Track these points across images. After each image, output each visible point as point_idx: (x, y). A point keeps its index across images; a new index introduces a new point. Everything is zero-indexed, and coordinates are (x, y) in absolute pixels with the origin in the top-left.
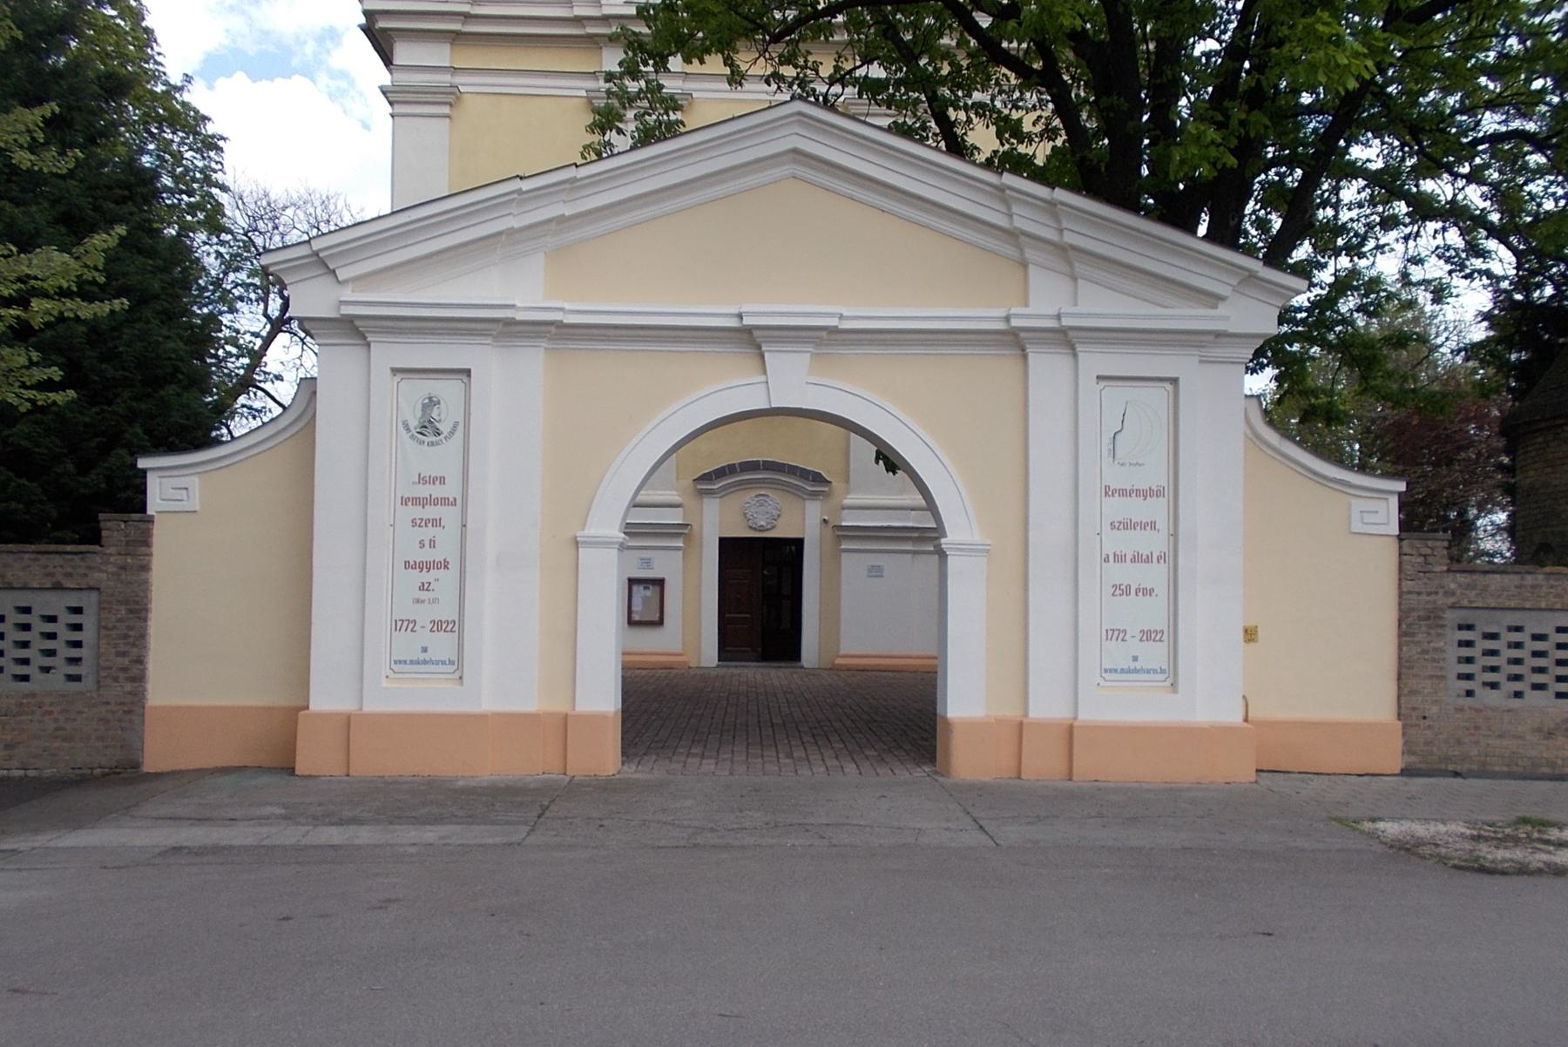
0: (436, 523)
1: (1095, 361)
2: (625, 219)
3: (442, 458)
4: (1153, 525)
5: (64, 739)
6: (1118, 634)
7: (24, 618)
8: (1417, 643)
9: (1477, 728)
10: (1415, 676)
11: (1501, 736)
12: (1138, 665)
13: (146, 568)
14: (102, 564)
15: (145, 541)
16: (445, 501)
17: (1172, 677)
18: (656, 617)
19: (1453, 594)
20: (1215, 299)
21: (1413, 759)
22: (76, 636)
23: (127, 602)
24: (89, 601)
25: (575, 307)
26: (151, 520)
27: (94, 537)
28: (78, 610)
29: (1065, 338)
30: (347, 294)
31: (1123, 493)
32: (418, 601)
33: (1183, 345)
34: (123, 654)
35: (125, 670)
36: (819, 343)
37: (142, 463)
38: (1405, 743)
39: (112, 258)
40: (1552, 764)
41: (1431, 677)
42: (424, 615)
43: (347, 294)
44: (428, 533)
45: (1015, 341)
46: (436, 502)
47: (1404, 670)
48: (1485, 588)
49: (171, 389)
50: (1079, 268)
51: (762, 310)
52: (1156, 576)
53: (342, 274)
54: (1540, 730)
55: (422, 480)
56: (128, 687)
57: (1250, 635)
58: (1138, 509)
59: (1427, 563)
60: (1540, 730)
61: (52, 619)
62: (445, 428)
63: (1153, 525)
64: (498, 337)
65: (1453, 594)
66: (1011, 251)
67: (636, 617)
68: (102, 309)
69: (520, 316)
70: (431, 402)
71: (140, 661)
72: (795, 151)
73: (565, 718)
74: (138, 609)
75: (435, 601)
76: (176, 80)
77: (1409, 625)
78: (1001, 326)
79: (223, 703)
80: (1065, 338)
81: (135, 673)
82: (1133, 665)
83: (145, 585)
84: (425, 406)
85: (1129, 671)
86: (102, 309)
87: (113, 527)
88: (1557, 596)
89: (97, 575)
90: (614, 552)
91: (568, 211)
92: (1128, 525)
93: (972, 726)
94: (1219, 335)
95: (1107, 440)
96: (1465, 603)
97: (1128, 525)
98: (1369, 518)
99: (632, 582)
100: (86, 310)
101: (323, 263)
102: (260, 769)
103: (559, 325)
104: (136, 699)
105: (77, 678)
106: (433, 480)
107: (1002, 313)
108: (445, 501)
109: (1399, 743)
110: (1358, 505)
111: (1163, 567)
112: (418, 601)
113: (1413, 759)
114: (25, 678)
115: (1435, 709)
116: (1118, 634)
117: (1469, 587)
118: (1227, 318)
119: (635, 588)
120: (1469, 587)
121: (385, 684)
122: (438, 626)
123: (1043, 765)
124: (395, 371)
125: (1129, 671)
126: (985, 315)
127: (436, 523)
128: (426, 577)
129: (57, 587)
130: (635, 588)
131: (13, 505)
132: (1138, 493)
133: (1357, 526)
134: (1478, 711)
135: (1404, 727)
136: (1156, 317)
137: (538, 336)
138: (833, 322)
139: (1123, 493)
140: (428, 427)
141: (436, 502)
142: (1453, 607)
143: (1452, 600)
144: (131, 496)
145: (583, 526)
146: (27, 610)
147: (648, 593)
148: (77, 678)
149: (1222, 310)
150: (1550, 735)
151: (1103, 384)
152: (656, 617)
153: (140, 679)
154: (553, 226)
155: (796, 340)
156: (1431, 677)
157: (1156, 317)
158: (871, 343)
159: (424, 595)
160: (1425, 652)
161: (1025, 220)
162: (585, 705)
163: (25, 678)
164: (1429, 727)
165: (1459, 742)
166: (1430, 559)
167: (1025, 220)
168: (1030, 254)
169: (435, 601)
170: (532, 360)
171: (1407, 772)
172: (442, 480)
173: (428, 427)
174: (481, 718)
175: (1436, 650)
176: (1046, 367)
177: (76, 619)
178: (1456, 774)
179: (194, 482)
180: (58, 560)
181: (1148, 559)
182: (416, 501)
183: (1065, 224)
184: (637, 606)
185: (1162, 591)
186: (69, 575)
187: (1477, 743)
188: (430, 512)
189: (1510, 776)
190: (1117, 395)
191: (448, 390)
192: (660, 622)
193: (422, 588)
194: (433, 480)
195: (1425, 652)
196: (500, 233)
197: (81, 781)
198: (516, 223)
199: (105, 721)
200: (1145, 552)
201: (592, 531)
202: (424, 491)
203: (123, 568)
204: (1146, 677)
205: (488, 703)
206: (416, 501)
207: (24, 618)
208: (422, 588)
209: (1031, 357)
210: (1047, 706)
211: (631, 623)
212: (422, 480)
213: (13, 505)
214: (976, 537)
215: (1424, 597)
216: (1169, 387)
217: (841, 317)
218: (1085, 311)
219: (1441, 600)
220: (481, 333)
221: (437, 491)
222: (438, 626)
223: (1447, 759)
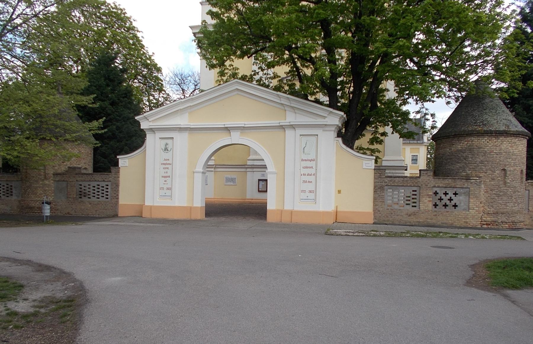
0: (168, 168)
1: (300, 131)
2: (212, 102)
3: (168, 155)
4: (312, 167)
5: (106, 210)
6: (304, 191)
7: (98, 187)
8: (378, 194)
9: (392, 214)
10: (377, 201)
11: (398, 216)
12: (308, 198)
13: (119, 177)
14: (111, 176)
15: (118, 172)
16: (169, 164)
17: (315, 200)
18: (266, 190)
19: (387, 183)
20: (325, 117)
21: (376, 220)
22: (107, 190)
23: (115, 184)
24: (109, 183)
25: (193, 125)
26: (119, 168)
27: (110, 172)
28: (107, 185)
29: (293, 127)
30: (151, 124)
31: (305, 160)
32: (164, 184)
33: (320, 127)
34: (115, 194)
35: (115, 197)
36: (242, 130)
37: (118, 157)
38: (374, 217)
39: (104, 122)
40: (410, 222)
41: (380, 202)
42: (165, 187)
43: (151, 124)
44: (166, 170)
45: (282, 127)
46: (167, 164)
47: (375, 199)
48: (394, 181)
49: (134, 138)
50: (296, 111)
51: (229, 123)
52: (312, 178)
53: (150, 120)
54: (407, 214)
55: (165, 160)
56: (116, 200)
57: (339, 192)
58: (309, 164)
59: (380, 175)
60: (407, 214)
61: (103, 187)
62: (169, 149)
63: (312, 167)
64: (179, 130)
65: (387, 183)
66: (283, 108)
67: (260, 190)
68: (103, 131)
69: (182, 127)
70: (167, 144)
71: (118, 195)
72: (237, 89)
73: (191, 207)
74: (117, 185)
75: (167, 184)
76: (150, 54)
77: (376, 190)
78: (278, 125)
79: (128, 203)
80: (293, 127)
81: (116, 197)
82: (307, 198)
83: (119, 180)
84: (165, 145)
85: (306, 199)
86: (103, 131)
87: (113, 169)
88: (412, 183)
89: (110, 179)
90: (201, 174)
91: (192, 105)
92: (307, 167)
93: (272, 211)
94: (326, 125)
95: (302, 149)
96: (389, 185)
97: (307, 167)
98: (367, 165)
99: (259, 180)
100: (100, 132)
101: (146, 118)
102: (138, 216)
103: (190, 128)
104: (117, 202)
105: (107, 198)
106: (167, 160)
107: (278, 122)
108: (169, 164)
109: (373, 216)
110: (364, 162)
111: (314, 176)
112: (164, 184)
113: (376, 220)
114: (99, 198)
115: (381, 209)
116: (304, 191)
117: (390, 181)
118: (327, 122)
119: (260, 182)
120: (390, 181)
121: (158, 200)
122: (168, 189)
123: (286, 219)
124: (160, 138)
125: (306, 199)
126: (275, 122)
127: (168, 168)
128: (166, 179)
129: (104, 181)
130: (260, 182)
131: (101, 164)
132: (309, 160)
133: (364, 167)
134: (392, 210)
135: (374, 213)
136: (315, 122)
137: (187, 130)
138: (243, 125)
139: (305, 160)
140: (166, 149)
141: (167, 164)
142: (386, 185)
143: (386, 184)
144: (116, 164)
145: (195, 169)
146: (99, 185)
147: (263, 183)
148: (107, 198)
149: (326, 119)
150: (410, 215)
151: (302, 136)
152: (266, 190)
153: (118, 199)
154: (189, 108)
155: (237, 129)
156: (380, 202)
157: (315, 122)
158: (253, 129)
159: (165, 183)
160: (380, 196)
161: (283, 101)
162: (195, 205)
163: (99, 198)
164: (380, 213)
165: (387, 217)
166: (381, 174)
167: (283, 101)
168: (286, 108)
169: (167, 184)
170: (185, 135)
171: (374, 223)
172: (169, 160)
173: (166, 149)
174: (175, 207)
175: (382, 195)
176: (289, 133)
177: (107, 187)
178: (386, 224)
179: (127, 160)
180: (104, 176)
181: (311, 175)
182: (164, 164)
183: (291, 102)
184: (260, 187)
185: (314, 182)
186: (106, 179)
187: (392, 217)
188: (166, 166)
189: (399, 225)
190: (304, 139)
191: (169, 142)
192: (267, 191)
193: (165, 181)
194: (167, 160)
195: (380, 196)
196: (188, 107)
197: (103, 218)
198: (181, 108)
199: (112, 206)
200: (310, 173)
201: (197, 170)
202: (165, 162)
203: (115, 177)
204: (310, 201)
205: (177, 204)
206: (164, 164)
207: (98, 187)
208: (165, 181)
209: (286, 131)
210: (288, 207)
211: (259, 191)
212: (165, 160)
213: (101, 164)
214: (274, 170)
215: (379, 183)
216: (316, 136)
217: (245, 124)
218: (297, 121)
219: (383, 184)
220: (175, 130)
221: (168, 162)
222: (168, 189)
223: (384, 221)
